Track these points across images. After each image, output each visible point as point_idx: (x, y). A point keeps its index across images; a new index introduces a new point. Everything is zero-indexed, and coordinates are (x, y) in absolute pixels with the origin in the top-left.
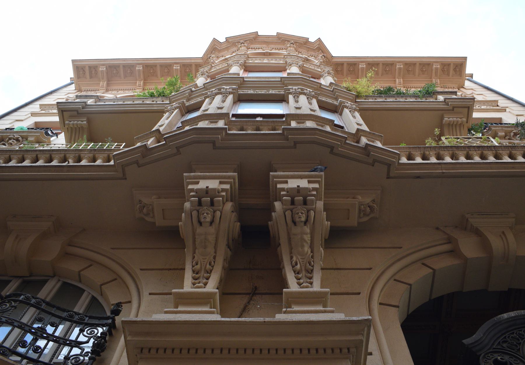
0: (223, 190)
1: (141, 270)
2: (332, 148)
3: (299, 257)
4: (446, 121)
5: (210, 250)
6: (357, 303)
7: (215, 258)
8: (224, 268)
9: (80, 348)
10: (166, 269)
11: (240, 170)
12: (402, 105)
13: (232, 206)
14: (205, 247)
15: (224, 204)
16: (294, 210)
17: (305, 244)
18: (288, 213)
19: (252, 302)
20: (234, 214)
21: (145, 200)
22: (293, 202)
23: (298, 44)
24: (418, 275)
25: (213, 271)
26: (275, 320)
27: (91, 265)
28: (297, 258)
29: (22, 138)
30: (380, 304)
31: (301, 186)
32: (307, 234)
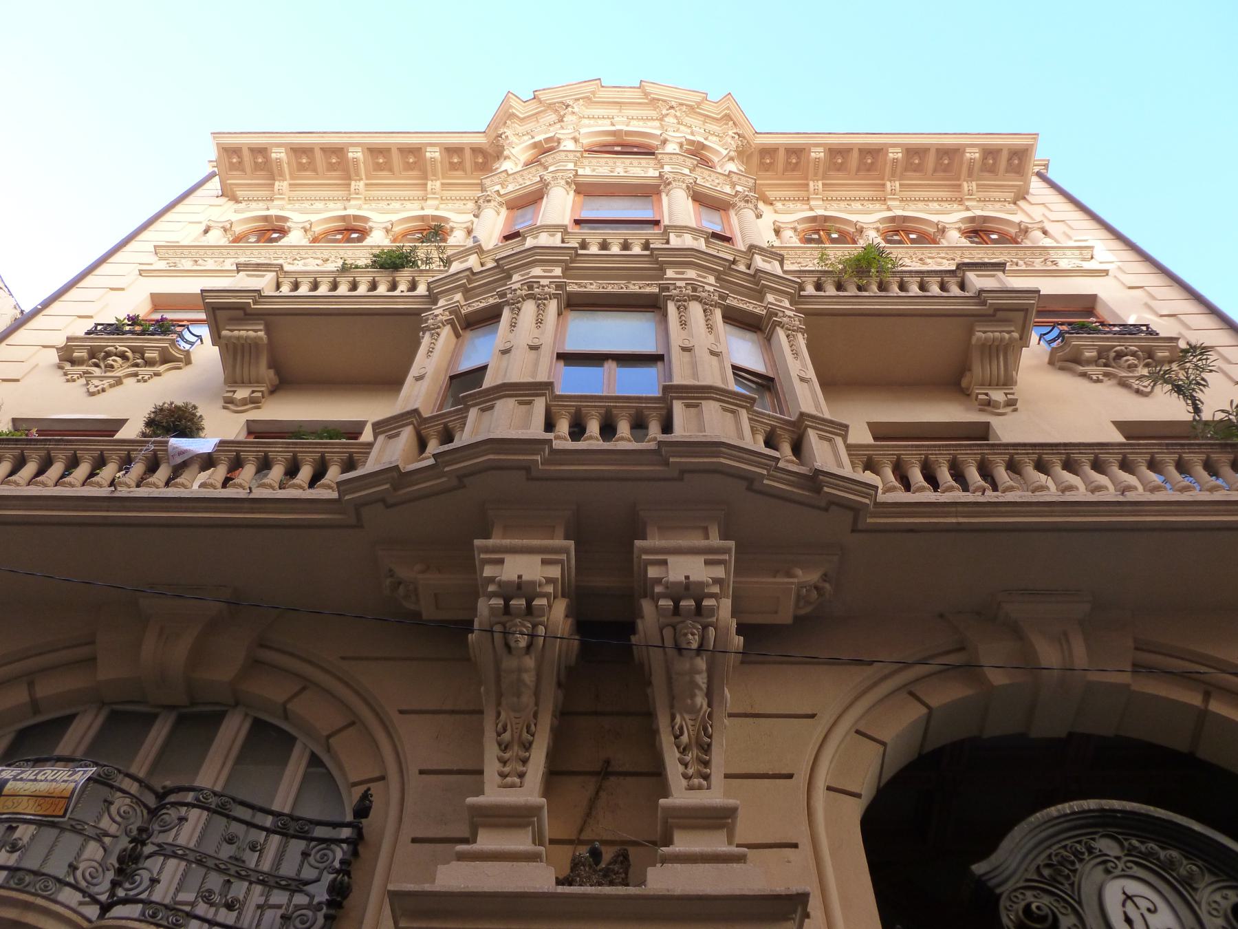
0: (549, 581)
1: (401, 712)
2: (750, 481)
3: (687, 717)
4: (979, 339)
5: (527, 699)
6: (784, 796)
7: (535, 715)
8: (552, 729)
9: (307, 895)
10: (445, 712)
11: (576, 532)
12: (893, 304)
13: (568, 606)
14: (519, 695)
15: (550, 606)
16: (679, 627)
17: (697, 691)
18: (668, 632)
19: (603, 794)
20: (570, 621)
21: (403, 573)
22: (676, 610)
23: (684, 108)
24: (900, 725)
25: (534, 746)
26: (646, 893)
27: (304, 689)
28: (683, 719)
29: (133, 352)
30: (829, 788)
31: (691, 579)
32: (699, 673)
